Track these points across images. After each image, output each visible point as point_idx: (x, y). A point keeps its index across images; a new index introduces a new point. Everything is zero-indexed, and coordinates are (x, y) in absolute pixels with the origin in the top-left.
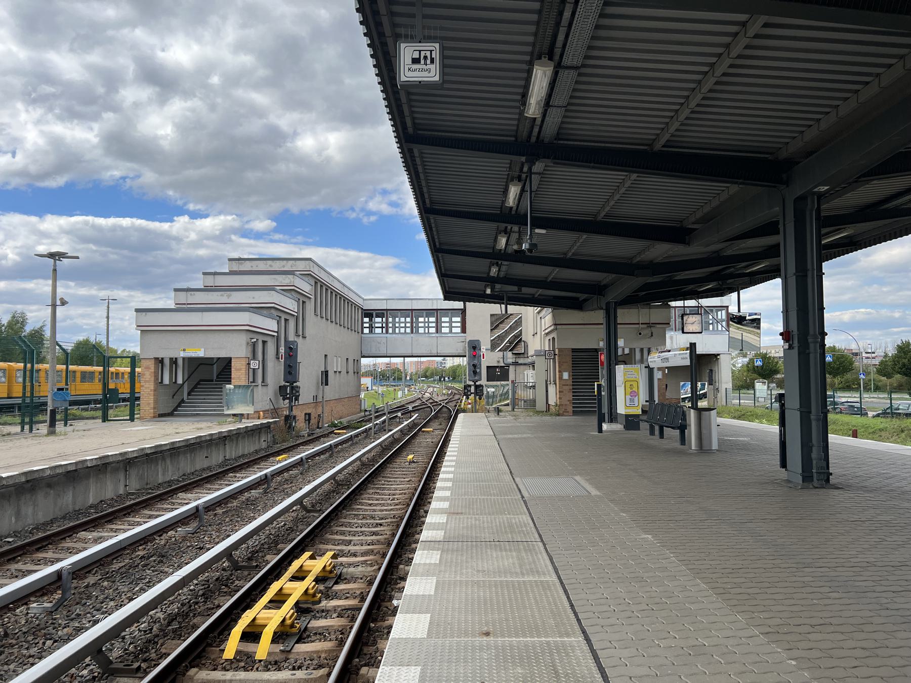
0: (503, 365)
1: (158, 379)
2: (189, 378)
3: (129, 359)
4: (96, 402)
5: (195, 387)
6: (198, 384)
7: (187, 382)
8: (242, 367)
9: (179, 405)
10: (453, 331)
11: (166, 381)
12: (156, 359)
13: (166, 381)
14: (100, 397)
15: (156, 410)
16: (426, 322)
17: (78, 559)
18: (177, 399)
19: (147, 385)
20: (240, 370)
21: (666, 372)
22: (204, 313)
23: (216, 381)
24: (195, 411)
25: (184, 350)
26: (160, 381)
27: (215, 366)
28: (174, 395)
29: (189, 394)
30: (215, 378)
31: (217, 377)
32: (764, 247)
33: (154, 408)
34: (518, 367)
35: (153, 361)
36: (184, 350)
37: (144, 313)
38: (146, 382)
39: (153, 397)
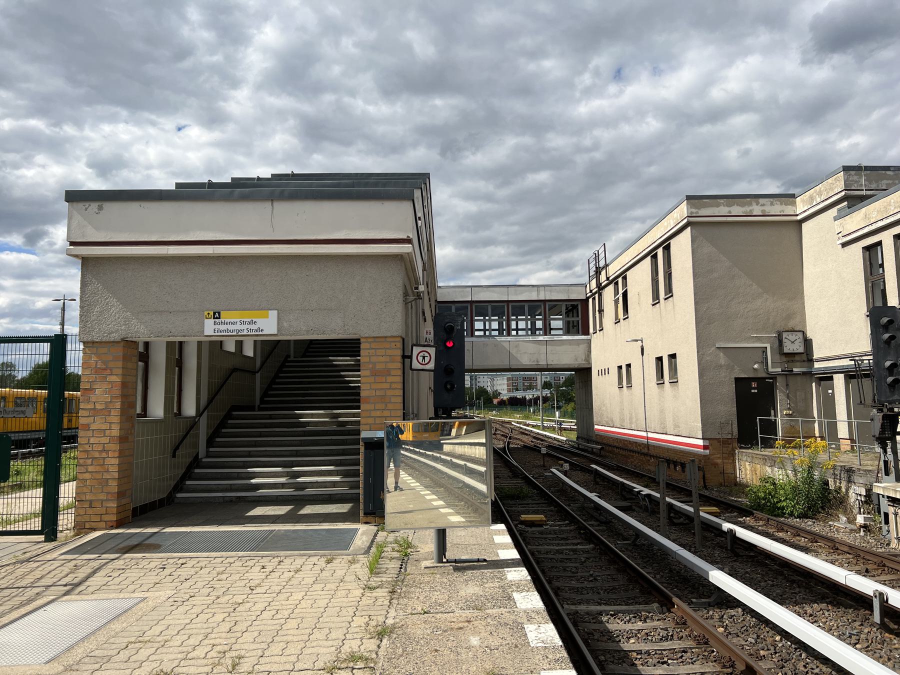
0: (764, 375)
1: (134, 406)
2: (210, 401)
3: (46, 347)
4: (39, 443)
5: (223, 424)
6: (229, 416)
7: (206, 413)
8: (390, 366)
9: (188, 474)
10: (406, 360)
11: (157, 409)
12: (128, 344)
13: (157, 409)
14: (42, 436)
15: (124, 501)
16: (488, 330)
18: (184, 457)
19: (98, 424)
20: (387, 372)
21: (753, 391)
22: (276, 204)
23: (260, 409)
24: (231, 489)
25: (217, 315)
26: (139, 410)
27: (258, 375)
28: (177, 448)
29: (210, 442)
30: (258, 402)
31: (262, 401)
33: (120, 495)
34: (791, 380)
35: (119, 351)
36: (217, 315)
37: (94, 206)
38: (95, 412)
39: (116, 461)
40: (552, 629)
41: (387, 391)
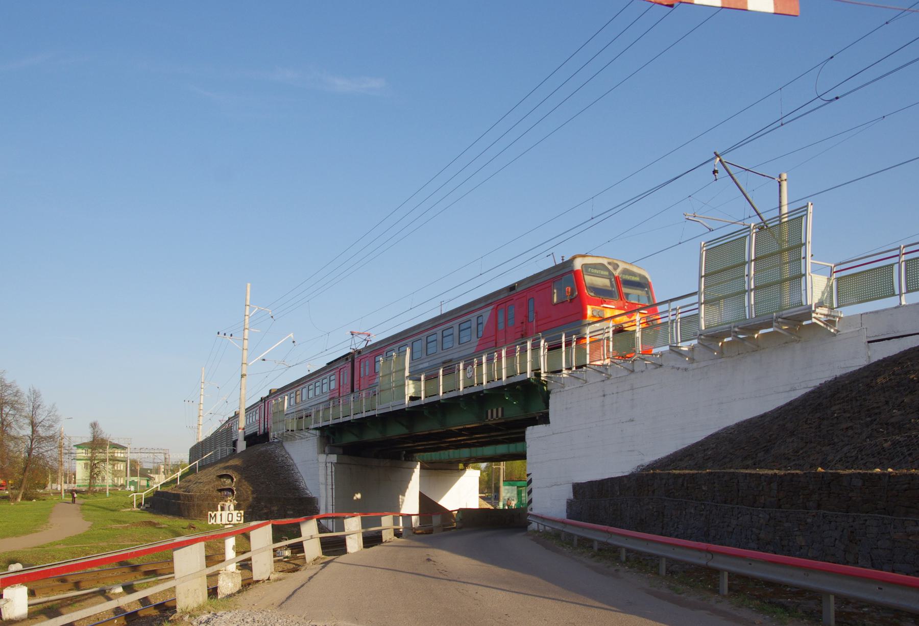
17: (293, 540)
32: (384, 546)
40: (512, 463)
41: (244, 362)
